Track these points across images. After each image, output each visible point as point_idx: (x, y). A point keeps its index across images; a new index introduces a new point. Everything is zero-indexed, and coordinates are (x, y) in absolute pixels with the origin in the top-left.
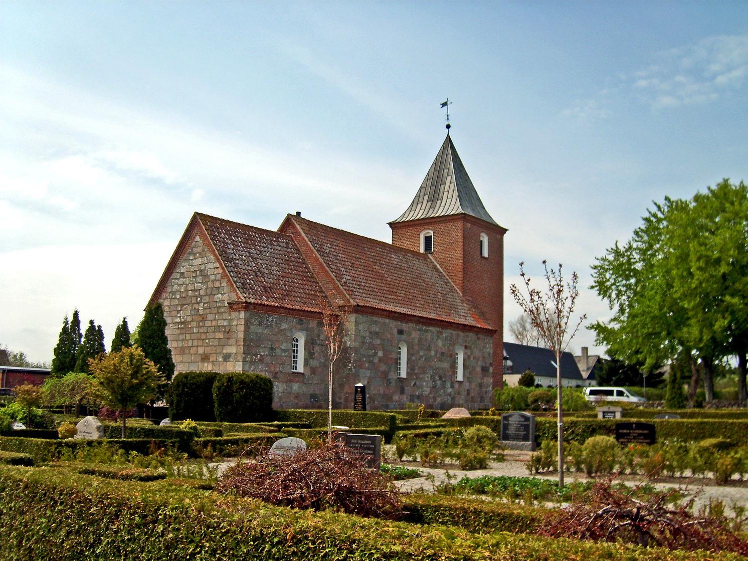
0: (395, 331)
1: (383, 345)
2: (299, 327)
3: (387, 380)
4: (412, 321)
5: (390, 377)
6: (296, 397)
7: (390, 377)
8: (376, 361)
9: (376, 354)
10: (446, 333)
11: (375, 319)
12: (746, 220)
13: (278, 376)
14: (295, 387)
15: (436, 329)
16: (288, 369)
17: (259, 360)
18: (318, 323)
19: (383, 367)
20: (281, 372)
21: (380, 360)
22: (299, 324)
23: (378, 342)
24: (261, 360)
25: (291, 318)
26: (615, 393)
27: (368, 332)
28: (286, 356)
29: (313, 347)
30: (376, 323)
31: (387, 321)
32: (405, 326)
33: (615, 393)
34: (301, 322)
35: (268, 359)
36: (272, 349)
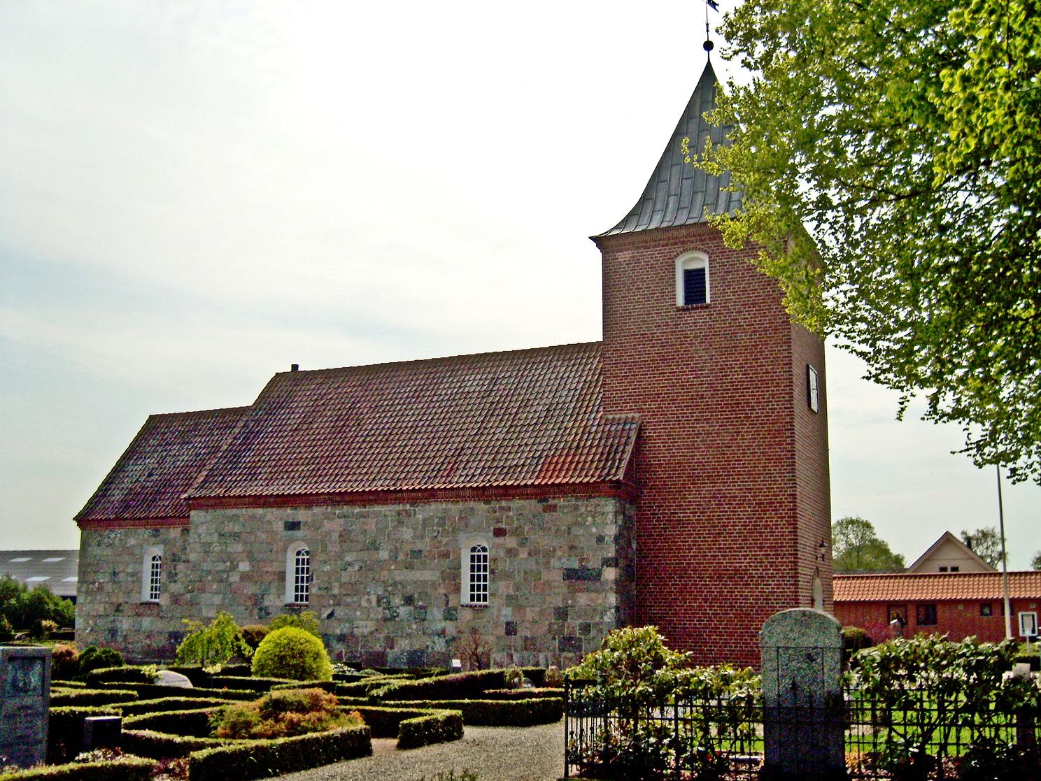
0: (279, 526)
1: (250, 552)
2: (153, 539)
3: (261, 609)
4: (319, 504)
5: (266, 603)
6: (148, 637)
7: (266, 603)
8: (235, 578)
9: (234, 568)
10: (425, 512)
11: (230, 512)
12: (1038, 358)
13: (121, 608)
14: (146, 623)
15: (391, 507)
16: (135, 599)
17: (98, 589)
18: (182, 531)
19: (250, 589)
20: (127, 603)
21: (245, 577)
22: (154, 536)
23: (239, 548)
24: (100, 589)
25: (142, 530)
26: (949, 569)
27: (216, 535)
28: (133, 582)
29: (175, 566)
30: (234, 518)
31: (260, 511)
32: (302, 515)
33: (949, 569)
34: (156, 533)
35: (108, 587)
36: (115, 574)
